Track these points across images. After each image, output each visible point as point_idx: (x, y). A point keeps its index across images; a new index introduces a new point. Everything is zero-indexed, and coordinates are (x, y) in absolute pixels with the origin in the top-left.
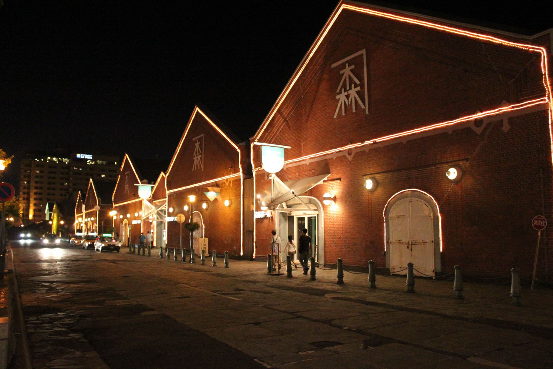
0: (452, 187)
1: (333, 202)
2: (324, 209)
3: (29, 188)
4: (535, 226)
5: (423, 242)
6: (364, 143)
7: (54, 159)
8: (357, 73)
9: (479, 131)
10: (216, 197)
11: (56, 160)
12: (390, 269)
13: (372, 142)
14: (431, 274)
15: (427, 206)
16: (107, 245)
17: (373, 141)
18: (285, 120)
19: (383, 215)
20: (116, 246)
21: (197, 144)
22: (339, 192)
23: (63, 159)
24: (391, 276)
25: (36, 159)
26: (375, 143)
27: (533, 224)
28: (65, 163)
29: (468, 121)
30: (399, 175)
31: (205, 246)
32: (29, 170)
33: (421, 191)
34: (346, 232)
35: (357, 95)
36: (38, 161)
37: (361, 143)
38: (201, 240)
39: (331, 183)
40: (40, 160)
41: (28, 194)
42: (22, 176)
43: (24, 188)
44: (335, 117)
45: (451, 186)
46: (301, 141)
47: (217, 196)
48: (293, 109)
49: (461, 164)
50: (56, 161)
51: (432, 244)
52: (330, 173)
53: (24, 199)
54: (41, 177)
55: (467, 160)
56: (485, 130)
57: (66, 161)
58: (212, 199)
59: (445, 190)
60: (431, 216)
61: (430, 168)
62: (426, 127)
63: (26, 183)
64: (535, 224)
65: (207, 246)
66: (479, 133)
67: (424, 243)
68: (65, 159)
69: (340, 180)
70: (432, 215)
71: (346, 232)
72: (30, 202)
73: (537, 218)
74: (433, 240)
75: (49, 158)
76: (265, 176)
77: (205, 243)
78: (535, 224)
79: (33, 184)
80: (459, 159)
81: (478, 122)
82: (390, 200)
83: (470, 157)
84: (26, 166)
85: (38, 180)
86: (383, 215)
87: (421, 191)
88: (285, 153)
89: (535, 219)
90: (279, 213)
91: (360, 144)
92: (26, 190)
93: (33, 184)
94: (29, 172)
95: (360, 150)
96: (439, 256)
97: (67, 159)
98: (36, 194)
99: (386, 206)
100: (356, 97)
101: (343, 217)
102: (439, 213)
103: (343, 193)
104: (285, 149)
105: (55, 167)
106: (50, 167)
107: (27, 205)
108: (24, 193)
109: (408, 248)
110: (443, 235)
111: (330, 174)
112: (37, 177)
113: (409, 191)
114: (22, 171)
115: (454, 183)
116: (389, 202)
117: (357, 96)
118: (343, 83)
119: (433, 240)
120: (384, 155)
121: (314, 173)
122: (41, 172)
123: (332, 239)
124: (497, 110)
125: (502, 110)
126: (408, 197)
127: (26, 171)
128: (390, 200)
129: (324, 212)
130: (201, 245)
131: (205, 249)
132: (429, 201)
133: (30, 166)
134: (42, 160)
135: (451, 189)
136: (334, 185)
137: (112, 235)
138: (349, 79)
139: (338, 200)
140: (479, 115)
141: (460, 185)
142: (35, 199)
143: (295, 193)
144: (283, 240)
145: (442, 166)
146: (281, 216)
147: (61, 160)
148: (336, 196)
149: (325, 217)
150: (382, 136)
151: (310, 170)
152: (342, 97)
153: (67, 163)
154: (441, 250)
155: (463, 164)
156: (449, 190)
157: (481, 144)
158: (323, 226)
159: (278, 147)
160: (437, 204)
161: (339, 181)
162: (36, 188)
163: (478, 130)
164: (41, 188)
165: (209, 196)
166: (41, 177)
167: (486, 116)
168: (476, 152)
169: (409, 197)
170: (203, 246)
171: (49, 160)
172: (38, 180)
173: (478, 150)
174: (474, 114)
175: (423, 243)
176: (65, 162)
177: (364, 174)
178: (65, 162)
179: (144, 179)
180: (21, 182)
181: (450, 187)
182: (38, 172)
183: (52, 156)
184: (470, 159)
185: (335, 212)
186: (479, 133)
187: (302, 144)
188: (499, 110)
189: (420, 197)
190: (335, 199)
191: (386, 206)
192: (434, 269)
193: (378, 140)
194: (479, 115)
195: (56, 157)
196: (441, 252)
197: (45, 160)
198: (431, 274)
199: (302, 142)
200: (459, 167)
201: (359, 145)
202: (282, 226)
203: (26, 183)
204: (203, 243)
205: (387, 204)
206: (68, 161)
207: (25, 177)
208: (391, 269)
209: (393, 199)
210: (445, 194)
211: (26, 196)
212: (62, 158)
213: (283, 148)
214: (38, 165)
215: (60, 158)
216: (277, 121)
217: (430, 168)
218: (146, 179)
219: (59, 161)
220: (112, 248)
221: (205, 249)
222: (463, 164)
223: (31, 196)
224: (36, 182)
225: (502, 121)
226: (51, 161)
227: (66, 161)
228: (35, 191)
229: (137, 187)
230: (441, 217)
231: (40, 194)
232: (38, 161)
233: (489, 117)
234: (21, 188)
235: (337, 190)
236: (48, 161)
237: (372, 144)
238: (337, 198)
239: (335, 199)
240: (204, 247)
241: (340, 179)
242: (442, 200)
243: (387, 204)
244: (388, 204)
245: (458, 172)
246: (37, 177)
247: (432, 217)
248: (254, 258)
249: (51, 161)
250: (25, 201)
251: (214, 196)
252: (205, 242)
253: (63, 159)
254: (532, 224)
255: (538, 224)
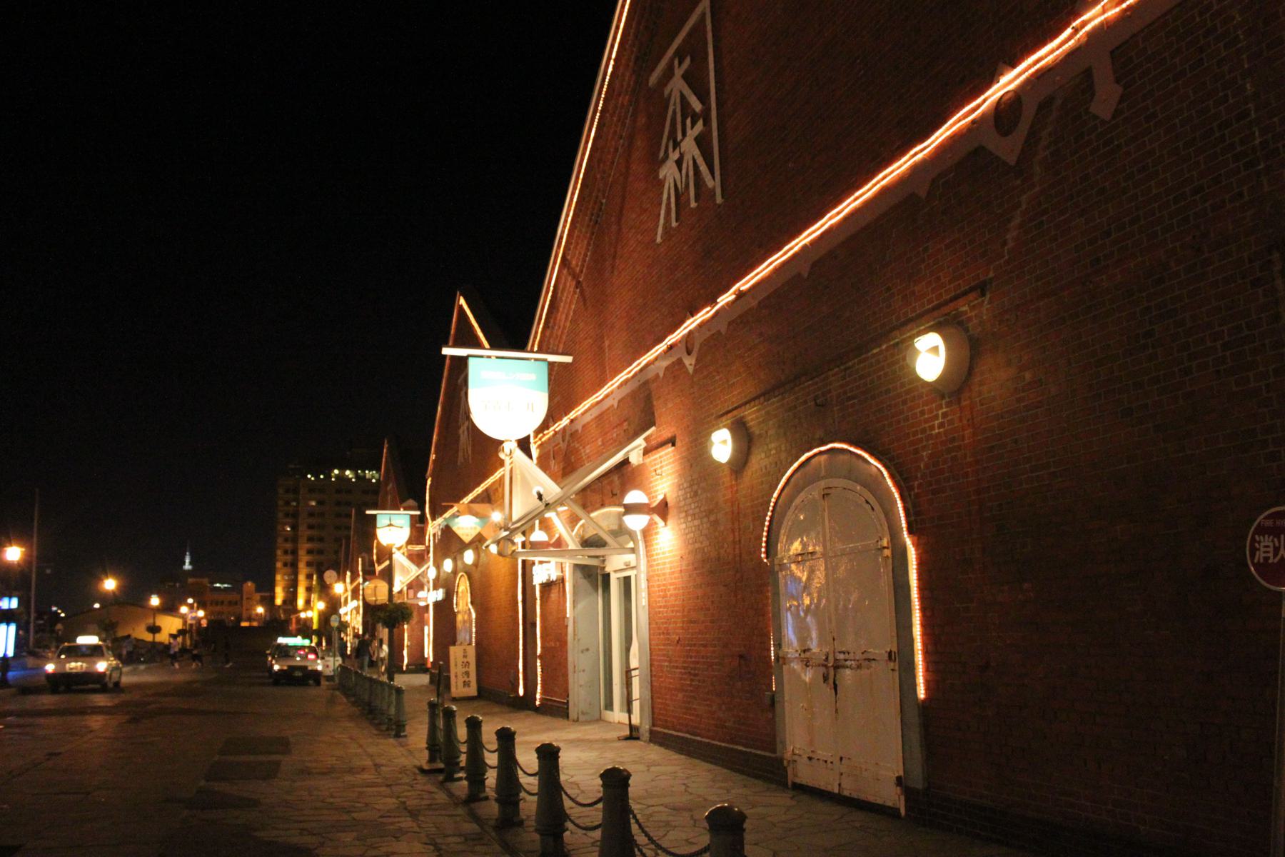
0: (944, 415)
1: (657, 518)
2: (646, 547)
3: (294, 539)
4: (1263, 567)
5: (865, 656)
6: (717, 303)
7: (348, 472)
8: (695, 80)
9: (1007, 149)
10: (478, 529)
11: (350, 476)
12: (785, 763)
13: (734, 296)
14: (891, 796)
15: (873, 509)
16: (285, 668)
17: (734, 293)
18: (578, 284)
19: (763, 556)
20: (310, 668)
21: (678, 85)
22: (673, 483)
23: (367, 472)
24: (788, 788)
25: (309, 476)
26: (740, 295)
27: (1253, 556)
28: (370, 480)
29: (973, 122)
30: (797, 399)
31: (467, 669)
32: (294, 501)
33: (852, 449)
34: (691, 622)
35: (698, 150)
36: (313, 479)
37: (709, 309)
38: (455, 653)
39: (657, 456)
40: (317, 477)
41: (294, 552)
42: (280, 515)
43: (286, 540)
44: (659, 240)
45: (940, 412)
46: (604, 338)
47: (483, 527)
48: (589, 244)
49: (966, 312)
50: (351, 479)
51: (891, 665)
52: (653, 424)
53: (285, 565)
54: (322, 515)
55: (982, 288)
56: (1033, 135)
57: (373, 477)
58: (468, 535)
59: (923, 431)
60: (884, 548)
61: (875, 351)
62: (857, 194)
63: (289, 529)
64: (1260, 556)
65: (473, 669)
66: (1012, 160)
67: (869, 660)
68: (371, 473)
69: (673, 445)
70: (885, 542)
71: (691, 622)
72: (299, 570)
73: (1269, 523)
74: (895, 649)
75: (336, 472)
76: (549, 458)
77: (465, 660)
78: (1260, 556)
79: (304, 532)
80: (958, 292)
81: (1006, 112)
82: (775, 495)
83: (991, 275)
84: (287, 491)
85: (312, 521)
86: (763, 556)
87: (852, 449)
88: (550, 374)
89: (1261, 530)
90: (572, 566)
91: (710, 310)
92: (289, 546)
93: (304, 532)
94: (294, 504)
95: (709, 330)
96: (914, 718)
97: (374, 472)
98: (310, 552)
99: (768, 518)
100: (696, 157)
101: (684, 568)
102: (905, 533)
103: (680, 486)
104: (551, 365)
105: (349, 492)
106: (339, 491)
107: (293, 577)
108: (286, 552)
109: (826, 679)
110: (924, 625)
111: (653, 429)
112: (311, 515)
113: (821, 453)
114: (281, 503)
115: (947, 400)
116: (776, 503)
117: (697, 153)
118: (671, 120)
119: (895, 649)
120: (761, 334)
121: (627, 429)
122: (320, 503)
123: (664, 645)
124: (1069, 31)
125: (1084, 24)
126: (819, 479)
127: (288, 503)
128: (775, 495)
129: (647, 556)
130: (456, 665)
131: (468, 677)
132: (873, 484)
133: (296, 491)
134: (322, 477)
135: (941, 425)
136: (663, 463)
137: (311, 642)
138: (682, 105)
139: (672, 513)
140: (1009, 82)
141: (968, 402)
142: (309, 564)
143: (544, 497)
144: (587, 650)
145: (908, 334)
146: (579, 575)
147: (362, 474)
148: (668, 500)
149: (648, 572)
150: (752, 268)
151: (620, 424)
152: (668, 172)
153: (374, 481)
154: (921, 693)
155: (973, 308)
156: (933, 432)
157: (1024, 207)
158: (644, 602)
159: (482, 357)
160: (897, 495)
161: (670, 449)
162: (310, 539)
163: (1007, 149)
164: (321, 540)
165: (459, 528)
166: (322, 515)
167: (1032, 75)
168: (1011, 244)
169: (823, 478)
170: (460, 666)
171: (337, 476)
172: (312, 521)
173: (1015, 234)
174: (989, 86)
175: (867, 662)
176: (370, 480)
177: (721, 413)
178: (370, 480)
179: (408, 499)
180: (279, 528)
181: (936, 417)
182: (313, 503)
183: (342, 469)
184: (991, 279)
185: (667, 555)
186: (1012, 160)
187: (607, 345)
188: (1076, 31)
189: (854, 473)
190: (663, 509)
191: (768, 518)
192: (901, 773)
193: (745, 284)
194: (1009, 82)
195: (354, 469)
196: (924, 701)
197: (328, 476)
198: (891, 796)
199: (605, 338)
200: (960, 323)
201: (705, 314)
202: (580, 606)
203: (289, 529)
204: (460, 660)
205: (769, 514)
206: (377, 476)
207: (287, 515)
208: (789, 761)
209: (785, 491)
210: (924, 448)
211: (289, 558)
212: (363, 471)
213: (544, 360)
214: (312, 488)
215: (359, 471)
216: (562, 293)
217: (875, 351)
218: (415, 500)
219: (357, 476)
220: (298, 674)
221: (468, 677)
222: (973, 308)
223: (299, 557)
224: (311, 527)
225: (1088, 73)
226: (341, 478)
227: (373, 477)
228: (309, 546)
229: (374, 517)
230: (917, 545)
231: (320, 552)
232: (313, 479)
233: (1043, 75)
234: (280, 540)
235: (670, 478)
236: (333, 479)
237: (734, 302)
238: (669, 505)
239: (663, 509)
240: (464, 670)
241: (672, 441)
242: (916, 478)
243: (769, 514)
244: (772, 511)
245: (948, 349)
246: (311, 515)
247: (887, 552)
248: (538, 703)
249: (341, 478)
250: (288, 570)
251: (475, 528)
252: (465, 656)
253: (367, 472)
254: (1249, 562)
255: (1275, 555)
